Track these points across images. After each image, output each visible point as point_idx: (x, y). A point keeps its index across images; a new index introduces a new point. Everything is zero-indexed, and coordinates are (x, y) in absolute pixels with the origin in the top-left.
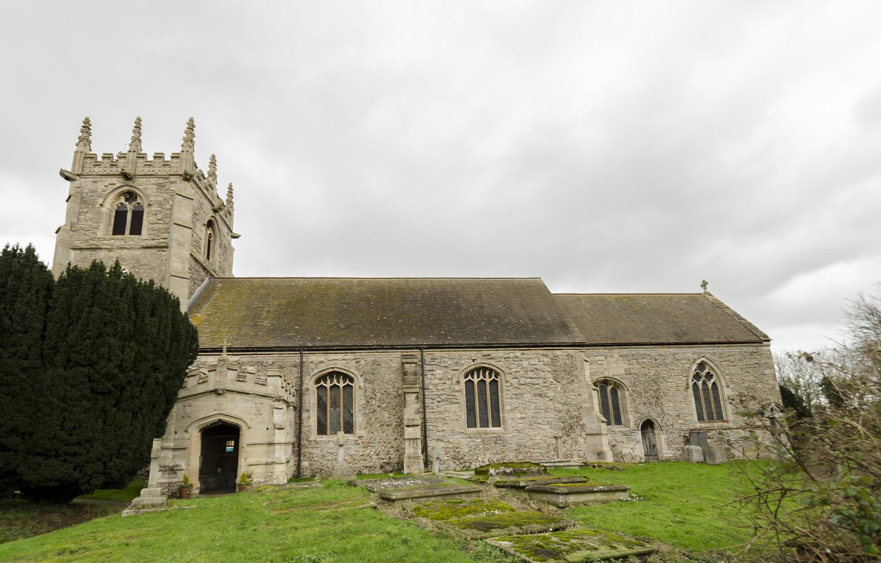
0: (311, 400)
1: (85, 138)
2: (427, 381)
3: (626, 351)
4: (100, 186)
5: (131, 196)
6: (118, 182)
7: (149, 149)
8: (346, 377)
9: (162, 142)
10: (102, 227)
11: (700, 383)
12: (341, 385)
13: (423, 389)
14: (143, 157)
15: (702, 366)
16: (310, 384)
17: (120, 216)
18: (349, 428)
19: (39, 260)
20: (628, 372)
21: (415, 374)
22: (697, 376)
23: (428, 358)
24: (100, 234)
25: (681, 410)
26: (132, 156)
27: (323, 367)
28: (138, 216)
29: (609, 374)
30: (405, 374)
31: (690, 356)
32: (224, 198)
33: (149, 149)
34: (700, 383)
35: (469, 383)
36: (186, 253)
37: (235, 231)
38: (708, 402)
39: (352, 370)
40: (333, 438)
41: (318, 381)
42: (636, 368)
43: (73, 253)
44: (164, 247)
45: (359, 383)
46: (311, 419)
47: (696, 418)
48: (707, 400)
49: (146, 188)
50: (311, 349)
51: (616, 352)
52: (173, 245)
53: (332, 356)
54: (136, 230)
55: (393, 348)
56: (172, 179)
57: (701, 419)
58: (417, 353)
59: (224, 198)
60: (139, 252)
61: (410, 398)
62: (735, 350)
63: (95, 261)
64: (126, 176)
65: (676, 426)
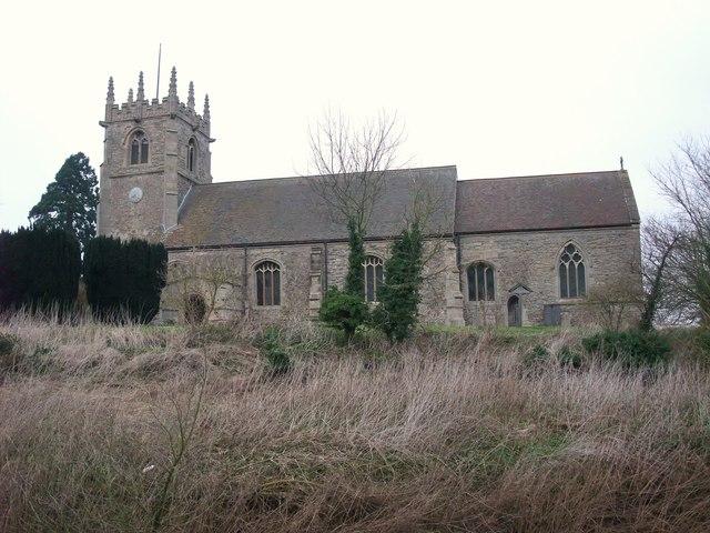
0: (253, 281)
1: (111, 95)
2: (329, 267)
3: (500, 237)
4: (122, 129)
5: (139, 133)
6: (132, 125)
7: (149, 96)
8: (275, 265)
9: (155, 91)
10: (125, 159)
11: (567, 265)
12: (374, 265)
13: (327, 273)
14: (146, 103)
15: (570, 248)
16: (251, 270)
17: (134, 148)
18: (277, 302)
19: (27, 224)
20: (501, 256)
21: (319, 262)
22: (565, 258)
23: (330, 250)
24: (124, 165)
25: (546, 285)
26: (139, 104)
27: (259, 258)
28: (145, 147)
29: (484, 257)
30: (313, 262)
31: (560, 239)
32: (202, 114)
33: (149, 96)
34: (567, 265)
35: (259, 273)
36: (174, 175)
37: (211, 137)
38: (572, 278)
39: (278, 259)
40: (268, 308)
41: (256, 268)
42: (509, 252)
43: (110, 181)
44: (161, 172)
45: (283, 269)
46: (253, 296)
47: (557, 293)
48: (572, 278)
49: (149, 127)
50: (253, 245)
51: (492, 239)
52: (166, 170)
53: (265, 251)
54: (145, 160)
55: (305, 242)
56: (164, 118)
57: (563, 295)
58: (322, 245)
59: (202, 114)
60: (147, 176)
61: (315, 280)
62: (604, 233)
63: (101, 123)
64: (137, 121)
65: (539, 301)
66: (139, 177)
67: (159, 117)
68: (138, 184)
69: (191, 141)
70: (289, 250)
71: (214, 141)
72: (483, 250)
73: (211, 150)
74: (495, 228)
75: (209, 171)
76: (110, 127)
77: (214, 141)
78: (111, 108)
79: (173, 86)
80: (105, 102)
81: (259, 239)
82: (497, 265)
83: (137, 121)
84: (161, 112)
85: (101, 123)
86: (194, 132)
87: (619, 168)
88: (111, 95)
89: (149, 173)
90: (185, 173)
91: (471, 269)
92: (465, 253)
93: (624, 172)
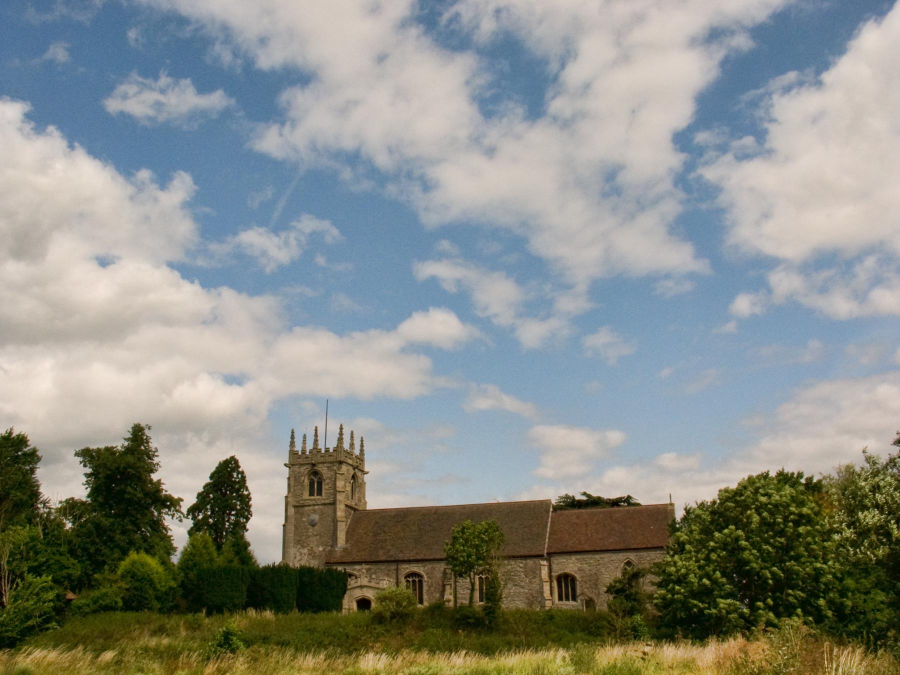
1: (292, 444)
27: (407, 571)
29: (567, 571)
37: (366, 470)
49: (323, 470)
60: (321, 507)
61: (448, 587)
66: (316, 507)
67: (332, 463)
68: (315, 511)
69: (353, 477)
70: (429, 566)
71: (367, 473)
72: (570, 565)
73: (365, 480)
74: (575, 549)
75: (364, 497)
76: (296, 468)
77: (367, 473)
78: (293, 453)
79: (340, 439)
80: (755, 474)
81: (411, 555)
82: (578, 576)
83: (314, 465)
84: (331, 459)
85: (285, 465)
86: (28, 117)
87: (668, 502)
88: (292, 444)
89: (323, 504)
90: (349, 503)
91: (559, 579)
92: (554, 567)
93: (672, 505)
